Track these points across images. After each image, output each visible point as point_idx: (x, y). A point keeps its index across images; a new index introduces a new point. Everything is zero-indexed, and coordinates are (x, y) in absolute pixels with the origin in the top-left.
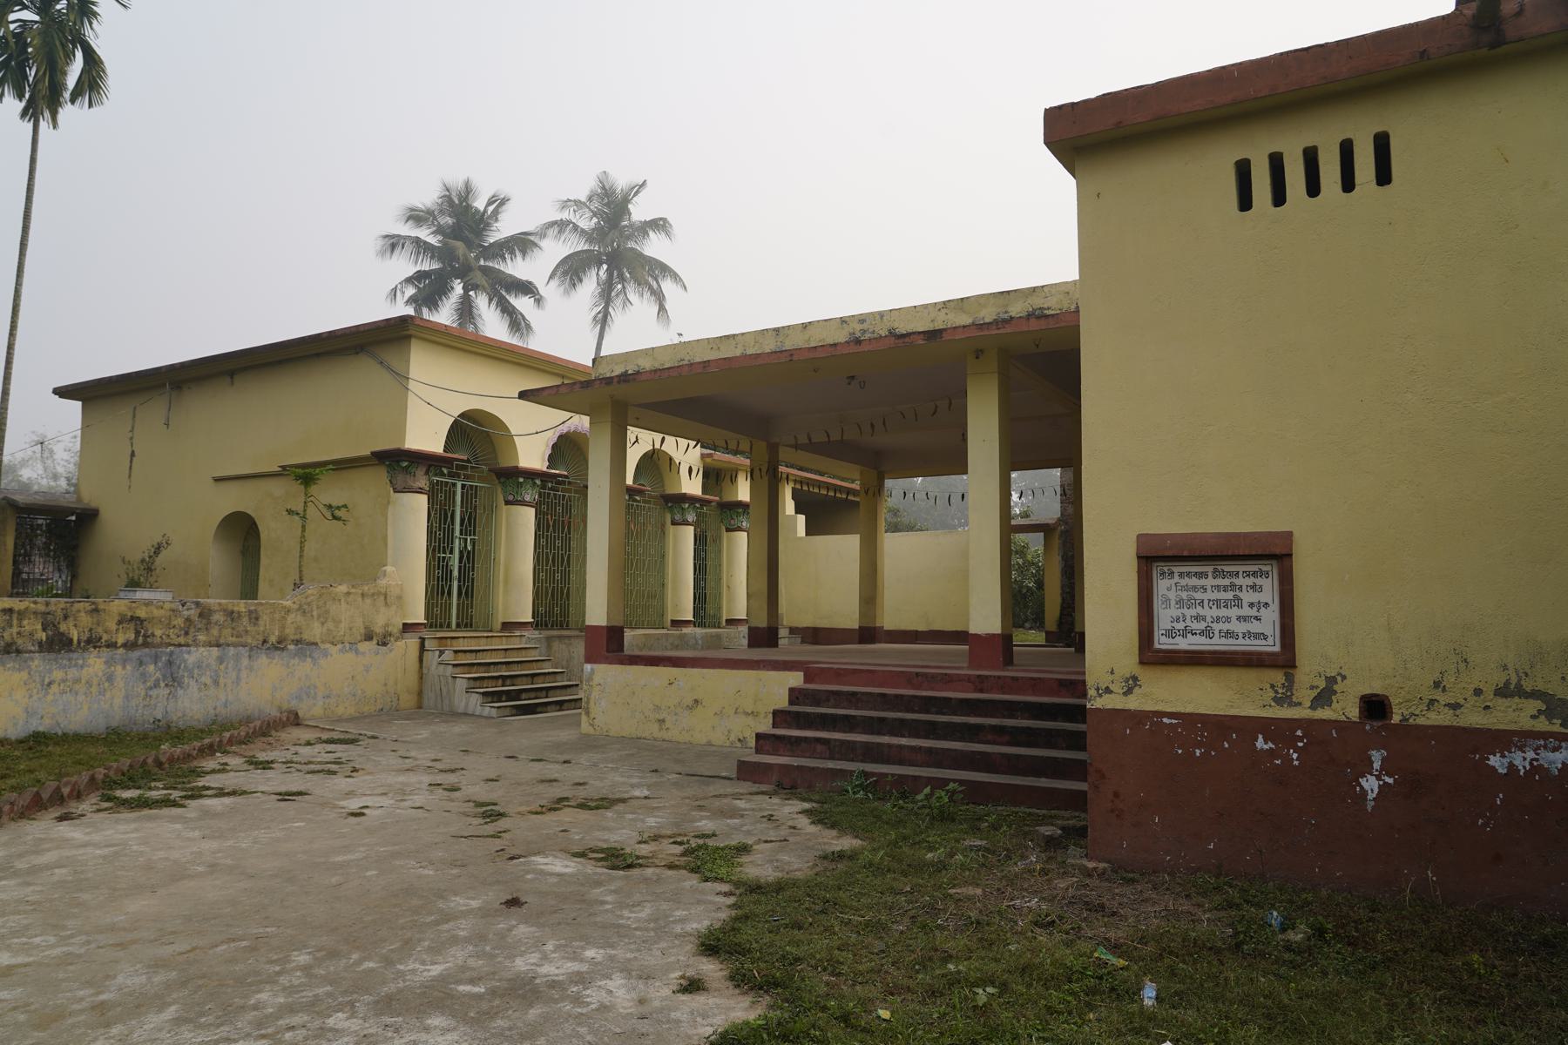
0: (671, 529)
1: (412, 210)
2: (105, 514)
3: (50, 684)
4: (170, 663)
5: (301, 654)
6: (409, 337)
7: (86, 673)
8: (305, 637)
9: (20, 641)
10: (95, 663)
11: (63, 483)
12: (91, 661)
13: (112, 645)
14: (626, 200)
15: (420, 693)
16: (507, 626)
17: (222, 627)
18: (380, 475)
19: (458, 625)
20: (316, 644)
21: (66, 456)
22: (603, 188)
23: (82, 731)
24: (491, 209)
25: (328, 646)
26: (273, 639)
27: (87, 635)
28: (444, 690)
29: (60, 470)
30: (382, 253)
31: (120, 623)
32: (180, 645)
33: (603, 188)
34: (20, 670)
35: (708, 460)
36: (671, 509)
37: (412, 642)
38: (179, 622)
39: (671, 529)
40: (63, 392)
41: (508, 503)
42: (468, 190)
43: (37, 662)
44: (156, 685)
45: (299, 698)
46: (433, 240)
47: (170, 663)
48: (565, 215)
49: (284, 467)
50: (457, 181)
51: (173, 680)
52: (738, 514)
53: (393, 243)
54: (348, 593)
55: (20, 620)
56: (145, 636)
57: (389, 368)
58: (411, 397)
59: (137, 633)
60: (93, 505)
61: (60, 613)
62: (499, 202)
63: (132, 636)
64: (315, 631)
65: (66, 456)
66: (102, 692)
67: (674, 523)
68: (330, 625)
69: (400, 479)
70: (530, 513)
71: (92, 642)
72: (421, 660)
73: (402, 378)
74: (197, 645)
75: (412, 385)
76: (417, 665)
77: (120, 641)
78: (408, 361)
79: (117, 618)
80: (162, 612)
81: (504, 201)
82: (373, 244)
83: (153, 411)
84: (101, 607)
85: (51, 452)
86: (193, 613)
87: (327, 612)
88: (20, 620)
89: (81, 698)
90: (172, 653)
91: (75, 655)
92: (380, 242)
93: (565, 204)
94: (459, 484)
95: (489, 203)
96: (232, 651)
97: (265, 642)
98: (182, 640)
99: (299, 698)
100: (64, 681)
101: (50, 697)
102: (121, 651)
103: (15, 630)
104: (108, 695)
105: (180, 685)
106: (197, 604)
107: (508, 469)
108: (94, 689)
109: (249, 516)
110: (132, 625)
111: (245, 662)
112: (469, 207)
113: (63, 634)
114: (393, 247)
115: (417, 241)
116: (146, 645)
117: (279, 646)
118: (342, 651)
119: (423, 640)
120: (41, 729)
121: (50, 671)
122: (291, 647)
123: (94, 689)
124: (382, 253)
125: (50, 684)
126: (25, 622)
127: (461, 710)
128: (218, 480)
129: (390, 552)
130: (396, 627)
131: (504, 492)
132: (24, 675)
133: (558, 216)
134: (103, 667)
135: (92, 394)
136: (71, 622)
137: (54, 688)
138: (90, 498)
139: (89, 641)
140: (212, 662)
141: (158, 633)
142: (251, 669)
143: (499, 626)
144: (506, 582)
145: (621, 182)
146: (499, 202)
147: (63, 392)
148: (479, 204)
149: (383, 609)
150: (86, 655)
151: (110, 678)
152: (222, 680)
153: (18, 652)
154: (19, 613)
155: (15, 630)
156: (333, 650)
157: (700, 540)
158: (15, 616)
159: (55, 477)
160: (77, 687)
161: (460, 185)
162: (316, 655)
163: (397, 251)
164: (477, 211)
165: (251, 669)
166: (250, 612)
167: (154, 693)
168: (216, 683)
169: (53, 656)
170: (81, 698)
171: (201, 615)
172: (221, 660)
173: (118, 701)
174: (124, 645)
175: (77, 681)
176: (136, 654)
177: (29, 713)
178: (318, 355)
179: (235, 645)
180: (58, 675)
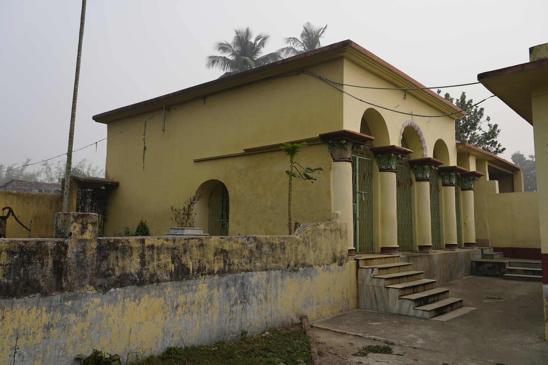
0: (443, 189)
1: (221, 44)
2: (123, 185)
3: (177, 306)
4: (243, 284)
5: (305, 274)
6: (342, 58)
7: (199, 294)
9: (159, 273)
10: (202, 287)
12: (200, 286)
13: (211, 273)
14: (317, 37)
15: (358, 298)
16: (384, 250)
18: (324, 150)
19: (360, 251)
20: (311, 266)
21: (56, 170)
22: (306, 30)
23: (196, 345)
24: (258, 42)
25: (317, 267)
26: (292, 264)
27: (197, 265)
28: (379, 297)
30: (208, 66)
31: (215, 255)
32: (247, 271)
33: (306, 30)
34: (159, 296)
35: (461, 147)
36: (442, 177)
37: (351, 264)
38: (246, 253)
39: (443, 189)
40: (98, 118)
41: (381, 170)
42: (248, 33)
43: (170, 288)
44: (236, 303)
45: (305, 306)
46: (231, 58)
47: (243, 284)
48: (289, 45)
49: (246, 150)
50: (243, 28)
52: (469, 180)
53: (213, 60)
54: (325, 230)
55: (158, 254)
56: (229, 265)
57: (326, 81)
58: (345, 96)
59: (225, 262)
60: (116, 180)
61: (181, 249)
62: (263, 40)
63: (222, 265)
64: (311, 258)
65: (56, 170)
66: (206, 312)
67: (444, 185)
68: (318, 252)
69: (337, 152)
70: (393, 176)
71: (201, 271)
73: (338, 86)
74: (256, 271)
75: (345, 89)
76: (355, 277)
77: (216, 269)
78: (342, 74)
79: (213, 251)
80: (238, 245)
81: (265, 39)
82: (204, 61)
83: (154, 125)
84: (205, 242)
85: (50, 168)
86: (252, 246)
87: (316, 243)
88: (158, 254)
89: (195, 316)
90: (243, 277)
91: (191, 282)
92: (208, 60)
93: (289, 40)
94: (357, 158)
95: (257, 39)
96: (273, 273)
97: (289, 266)
98: (248, 267)
99: (305, 306)
100: (185, 304)
101: (177, 318)
102: (217, 277)
103: (156, 263)
104: (210, 312)
106: (255, 238)
108: (202, 309)
109: (223, 184)
110: (222, 257)
111: (280, 281)
113: (183, 265)
114: (213, 62)
115: (225, 59)
116: (230, 271)
118: (324, 271)
119: (357, 261)
120: (172, 345)
122: (301, 269)
123: (202, 309)
124: (208, 66)
125: (177, 306)
126: (162, 256)
128: (196, 161)
129: (332, 201)
130: (345, 254)
131: (379, 164)
132: (162, 300)
133: (286, 46)
134: (207, 290)
135: (110, 118)
137: (180, 309)
138: (114, 178)
139: (199, 270)
140: (264, 282)
141: (236, 261)
142: (282, 287)
143: (380, 250)
144: (383, 221)
145: (316, 26)
146: (263, 40)
147: (98, 118)
151: (211, 299)
152: (269, 296)
153: (158, 281)
155: (156, 263)
156: (320, 269)
158: (155, 251)
159: (52, 179)
160: (192, 308)
161: (244, 30)
163: (215, 64)
164: (251, 43)
167: (234, 309)
168: (266, 298)
169: (178, 283)
170: (195, 316)
171: (257, 247)
172: (268, 280)
173: (216, 317)
174: (218, 272)
175: (193, 303)
176: (225, 279)
177: (165, 332)
178: (267, 79)
179: (275, 269)
180: (181, 299)
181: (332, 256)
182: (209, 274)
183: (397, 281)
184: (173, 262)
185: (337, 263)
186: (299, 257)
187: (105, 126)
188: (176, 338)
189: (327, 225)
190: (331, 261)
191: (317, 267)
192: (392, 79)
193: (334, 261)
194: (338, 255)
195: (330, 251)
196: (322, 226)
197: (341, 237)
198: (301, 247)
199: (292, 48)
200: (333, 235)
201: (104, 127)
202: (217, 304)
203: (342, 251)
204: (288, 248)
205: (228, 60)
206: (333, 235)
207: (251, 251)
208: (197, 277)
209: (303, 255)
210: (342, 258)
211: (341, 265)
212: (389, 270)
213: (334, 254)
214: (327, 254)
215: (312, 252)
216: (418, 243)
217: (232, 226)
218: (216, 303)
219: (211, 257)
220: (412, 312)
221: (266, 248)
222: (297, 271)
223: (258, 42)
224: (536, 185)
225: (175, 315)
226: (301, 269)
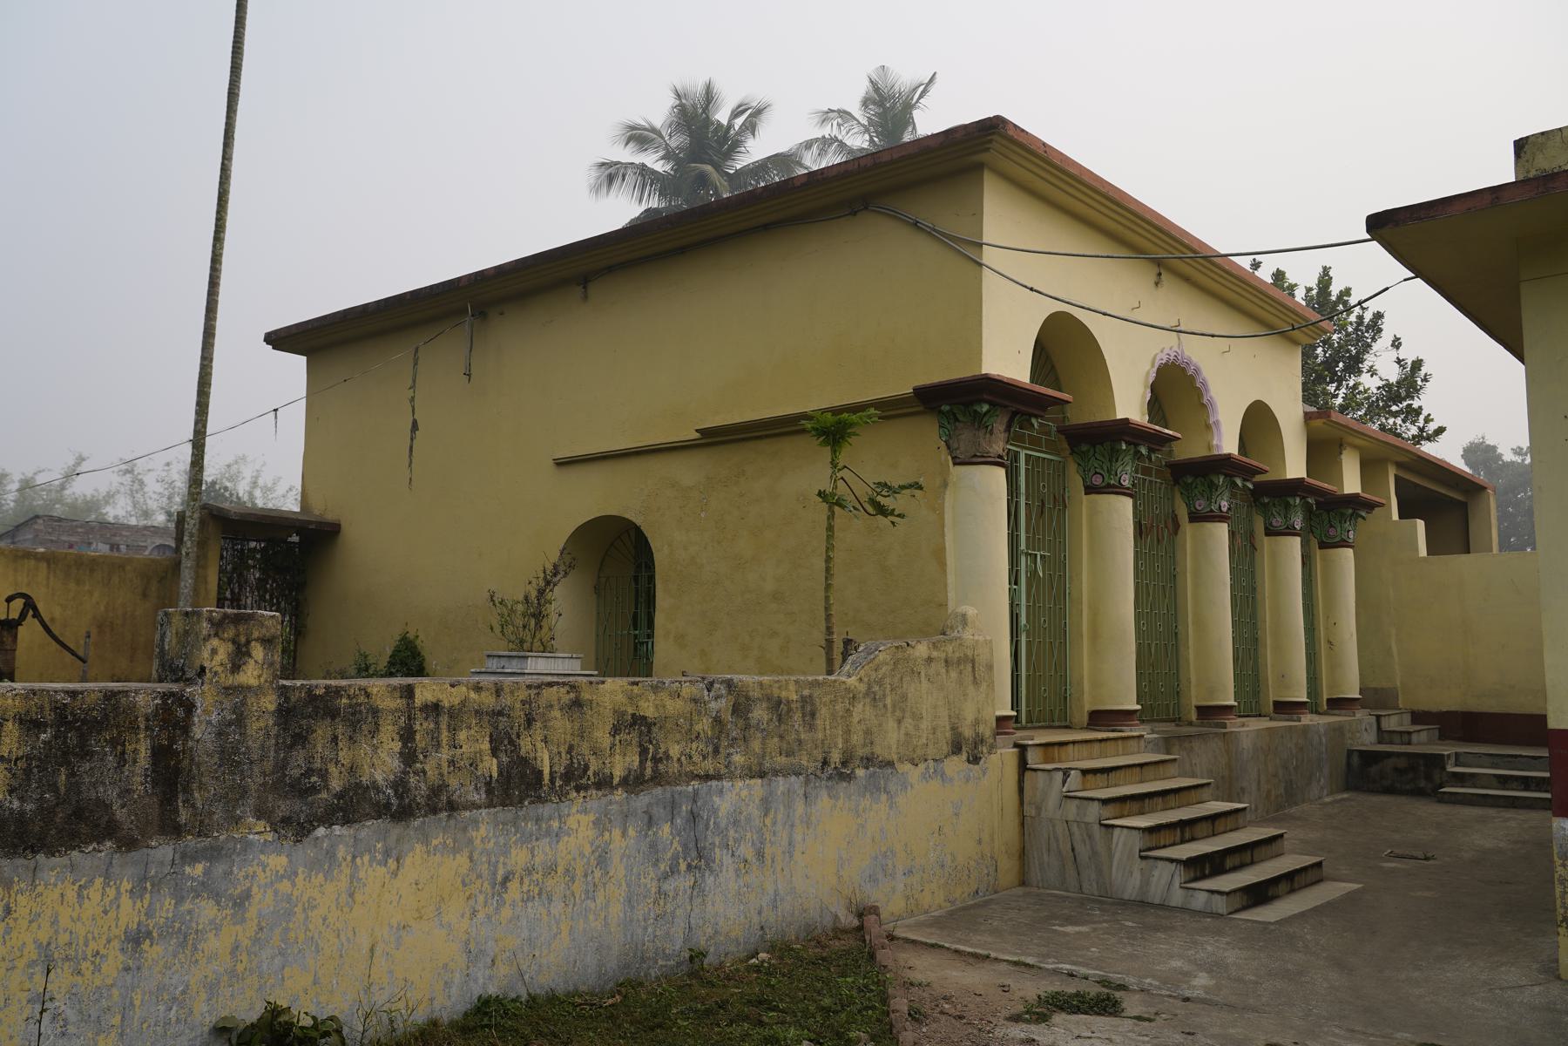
1: (632, 128)
2: (350, 532)
3: (506, 879)
4: (694, 817)
5: (873, 788)
6: (979, 168)
7: (568, 845)
8: (878, 750)
9: (453, 782)
10: (578, 824)
11: (160, 519)
12: (571, 822)
14: (908, 107)
15: (1023, 854)
16: (1099, 718)
17: (766, 735)
18: (927, 433)
19: (1030, 720)
20: (890, 764)
21: (159, 488)
22: (876, 89)
23: (560, 990)
24: (739, 122)
25: (908, 767)
26: (836, 757)
28: (1083, 852)
29: (152, 505)
30: (596, 189)
31: (616, 731)
32: (707, 777)
34: (455, 851)
35: (1318, 423)
36: (1265, 510)
37: (1003, 758)
38: (704, 725)
39: (1266, 543)
40: (280, 340)
41: (1090, 489)
42: (709, 96)
43: (485, 828)
44: (673, 870)
46: (661, 167)
47: (694, 817)
48: (826, 131)
49: (704, 432)
51: (699, 858)
52: (1343, 518)
53: (611, 174)
54: (930, 660)
55: (453, 730)
57: (932, 234)
59: (643, 752)
60: (330, 517)
61: (519, 714)
62: (753, 116)
64: (890, 740)
65: (159, 488)
66: (590, 895)
67: (1270, 532)
68: (908, 723)
69: (965, 437)
70: (1125, 505)
71: (575, 778)
72: (1021, 790)
73: (968, 250)
74: (732, 777)
75: (989, 256)
77: (618, 773)
78: (978, 215)
79: (610, 721)
82: (585, 175)
83: (441, 357)
84: (585, 696)
85: (142, 483)
86: (722, 705)
87: (904, 698)
88: (453, 730)
89: (557, 907)
91: (546, 810)
92: (594, 174)
93: (826, 116)
95: (736, 114)
96: (781, 784)
97: (825, 763)
98: (709, 766)
99: (873, 879)
100: (529, 871)
101: (506, 912)
102: (619, 795)
103: (445, 754)
105: (709, 862)
106: (729, 684)
107: (1102, 425)
108: (578, 887)
111: (800, 807)
112: (707, 121)
113: (524, 761)
114: (611, 179)
115: (643, 170)
116: (658, 779)
117: (843, 774)
118: (925, 777)
119: (1022, 749)
120: (492, 990)
121: (506, 851)
122: (860, 772)
123: (578, 887)
124: (596, 189)
125: (506, 879)
126: (462, 735)
127: (1157, 901)
128: (562, 463)
130: (987, 730)
132: (462, 859)
133: (818, 133)
134: (591, 833)
135: (315, 340)
136: (538, 730)
137: (514, 891)
138: (324, 509)
139: (568, 776)
141: (675, 751)
142: (807, 823)
143: (1086, 719)
144: (1095, 635)
145: (904, 76)
146: (753, 116)
147: (280, 340)
148: (722, 116)
149: (971, 689)
150: (564, 808)
151: (602, 859)
152: (768, 851)
153: (452, 807)
154: (454, 714)
155: (445, 754)
156: (913, 773)
157: (1307, 561)
158: (444, 720)
159: (146, 514)
160: (550, 883)
161: (700, 88)
162: (892, 787)
164: (719, 124)
165: (807, 823)
166: (804, 700)
167: (669, 886)
168: (760, 855)
170: (557, 907)
171: (736, 710)
172: (766, 805)
173: (616, 910)
174: (624, 782)
175: (551, 869)
176: (642, 801)
177: (472, 954)
178: (766, 227)
180: (518, 857)
181: (948, 734)
182: (599, 785)
183: (1135, 806)
184: (494, 752)
185: (964, 756)
186: (856, 739)
187: (302, 360)
188: (503, 970)
189: (935, 646)
190: (946, 749)
191: (906, 767)
192: (1120, 228)
193: (956, 748)
194: (968, 732)
195: (944, 722)
196: (922, 650)
197: (975, 682)
198: (861, 710)
199: (836, 139)
200: (954, 674)
201: (296, 364)
202: (621, 872)
203: (977, 722)
204: (823, 712)
205: (654, 172)
206: (954, 674)
207: (717, 721)
208: (562, 795)
209: (868, 732)
210: (979, 741)
211: (975, 760)
212: (1112, 775)
213: (953, 729)
214: (934, 730)
215: (891, 724)
216: (1196, 697)
217: (663, 648)
218: (618, 869)
219: (603, 737)
220: (1177, 897)
221: (759, 713)
222: (849, 778)
223: (739, 122)
224: (1532, 534)
225: (501, 903)
226: (860, 772)
